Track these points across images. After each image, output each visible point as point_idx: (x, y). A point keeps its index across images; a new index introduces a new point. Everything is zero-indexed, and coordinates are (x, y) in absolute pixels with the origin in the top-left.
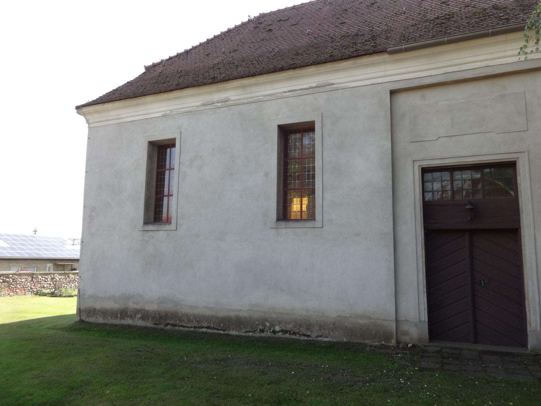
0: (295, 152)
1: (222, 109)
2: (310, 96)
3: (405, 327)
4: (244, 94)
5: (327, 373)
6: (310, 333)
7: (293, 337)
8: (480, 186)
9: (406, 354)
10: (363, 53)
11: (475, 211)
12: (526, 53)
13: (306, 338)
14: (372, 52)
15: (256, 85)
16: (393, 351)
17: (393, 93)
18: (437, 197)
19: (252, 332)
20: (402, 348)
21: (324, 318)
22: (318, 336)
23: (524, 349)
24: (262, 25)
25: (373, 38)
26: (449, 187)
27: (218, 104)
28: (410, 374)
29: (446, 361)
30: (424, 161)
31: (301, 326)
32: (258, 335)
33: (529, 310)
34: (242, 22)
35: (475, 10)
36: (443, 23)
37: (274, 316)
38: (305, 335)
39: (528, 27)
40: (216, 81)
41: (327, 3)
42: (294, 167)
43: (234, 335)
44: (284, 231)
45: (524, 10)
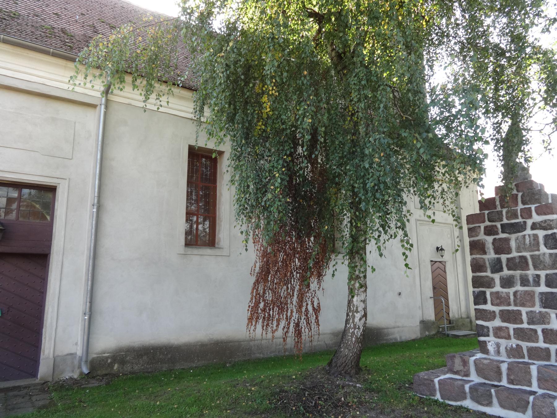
8: (14, 206)
12: (75, 85)
23: (34, 379)
33: (45, 338)
35: (43, 23)
36: (5, 19)
39: (79, 60)
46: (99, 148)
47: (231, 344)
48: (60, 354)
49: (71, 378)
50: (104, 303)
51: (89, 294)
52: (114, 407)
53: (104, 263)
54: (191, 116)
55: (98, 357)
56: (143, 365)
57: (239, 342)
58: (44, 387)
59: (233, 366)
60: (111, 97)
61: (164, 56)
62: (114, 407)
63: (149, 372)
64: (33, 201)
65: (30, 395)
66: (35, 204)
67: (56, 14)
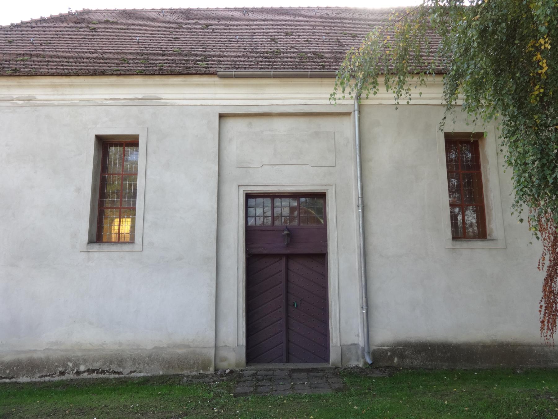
0: (115, 168)
1: (24, 108)
2: (135, 108)
3: (223, 353)
4: (54, 95)
5: (136, 413)
6: (121, 370)
7: (102, 376)
8: (296, 214)
9: (223, 381)
10: (194, 72)
11: (291, 236)
12: (335, 99)
13: (117, 376)
14: (203, 72)
15: (71, 86)
16: (210, 379)
17: (221, 116)
18: (259, 222)
19: (49, 376)
20: (220, 375)
21: (139, 351)
22: (131, 372)
23: (327, 363)
24: (83, 20)
25: (206, 59)
26: (269, 213)
27: (18, 102)
28: (225, 402)
29: (260, 383)
30: (248, 187)
31: (111, 362)
32: (56, 378)
33: (332, 328)
34: (60, 14)
35: (298, 52)
36: (271, 58)
37: (79, 354)
38: (115, 373)
40: (18, 74)
41: (161, 15)
42: (113, 186)
43: (24, 383)
44: (96, 255)
45: (336, 60)
46: (358, 152)
47: (519, 347)
48: (345, 344)
49: (357, 367)
50: (379, 298)
51: (364, 289)
52: (401, 399)
53: (375, 260)
54: (439, 102)
55: (378, 349)
56: (422, 362)
57: (530, 346)
58: (336, 371)
59: (527, 373)
60: (365, 102)
61: (414, 48)
62: (401, 399)
63: (430, 369)
64: (309, 208)
65: (327, 378)
66: (310, 210)
67: (307, 41)
